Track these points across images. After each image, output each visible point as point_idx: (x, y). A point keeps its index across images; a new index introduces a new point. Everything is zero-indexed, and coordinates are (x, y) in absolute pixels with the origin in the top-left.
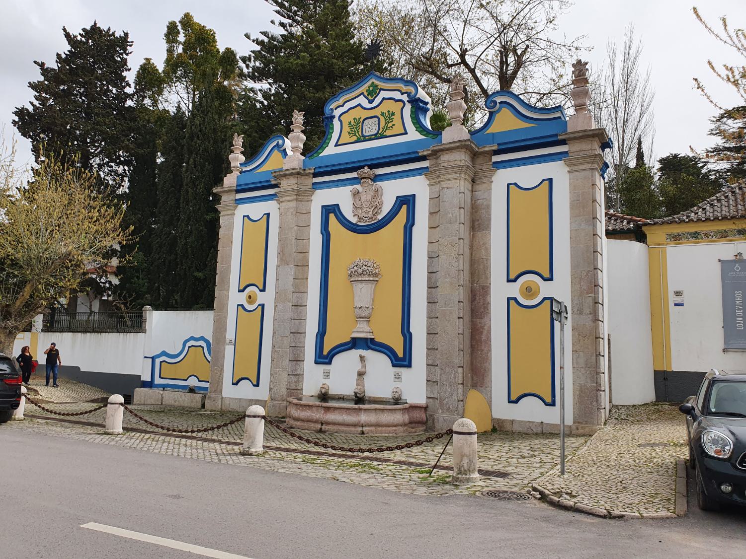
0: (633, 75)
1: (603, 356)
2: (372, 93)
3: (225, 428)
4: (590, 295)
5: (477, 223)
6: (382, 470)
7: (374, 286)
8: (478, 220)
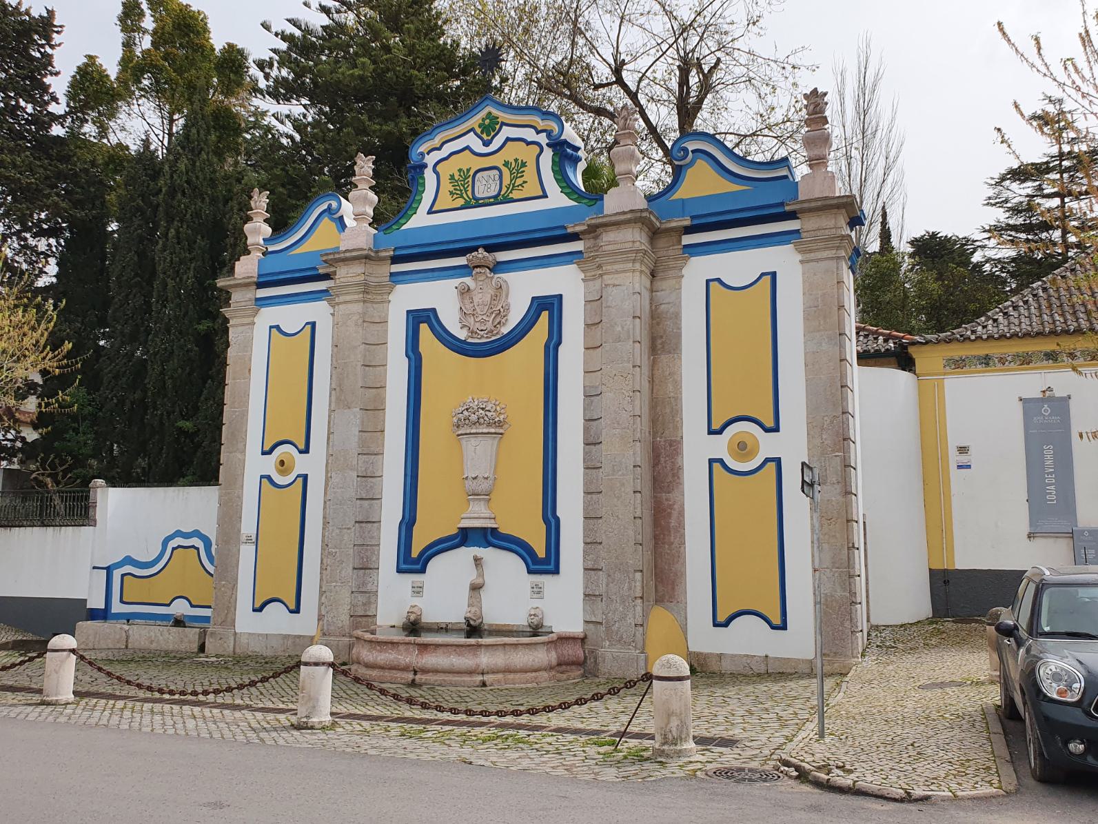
0: (872, 111)
1: (858, 549)
2: (489, 129)
3: (253, 689)
4: (837, 454)
5: (659, 341)
6: (536, 743)
7: (497, 440)
8: (662, 337)
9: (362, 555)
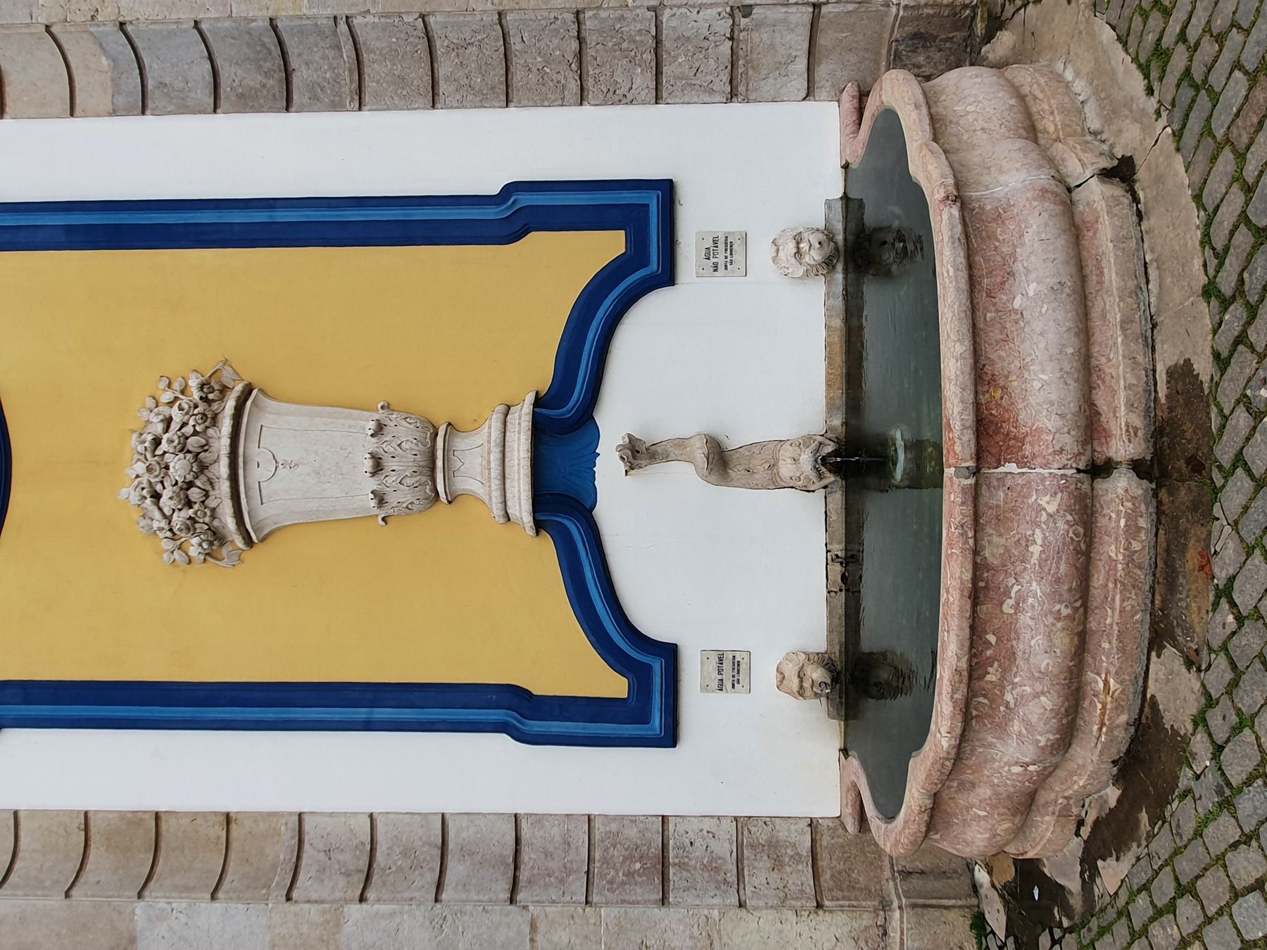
9: (621, 877)
